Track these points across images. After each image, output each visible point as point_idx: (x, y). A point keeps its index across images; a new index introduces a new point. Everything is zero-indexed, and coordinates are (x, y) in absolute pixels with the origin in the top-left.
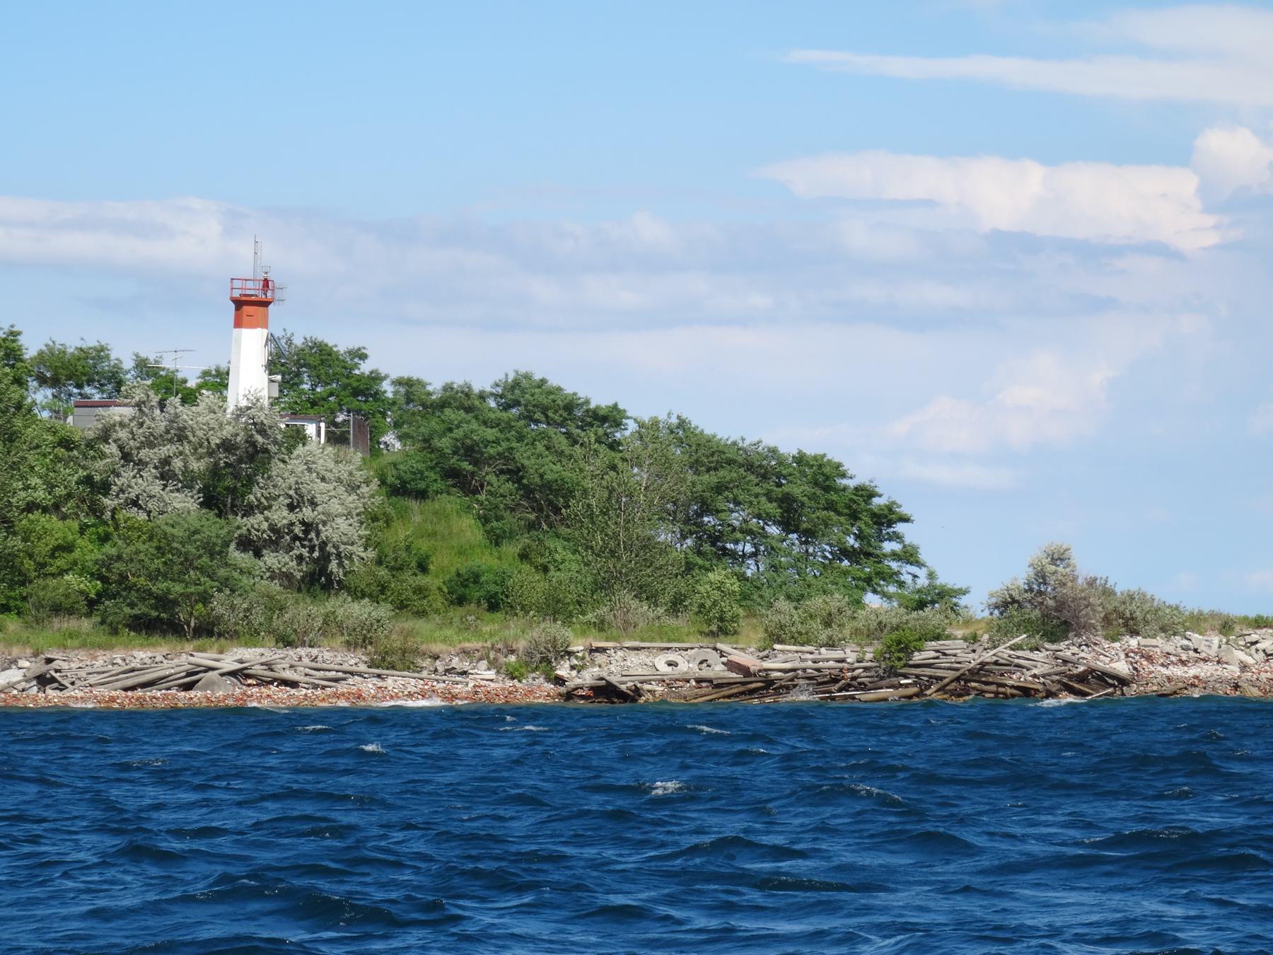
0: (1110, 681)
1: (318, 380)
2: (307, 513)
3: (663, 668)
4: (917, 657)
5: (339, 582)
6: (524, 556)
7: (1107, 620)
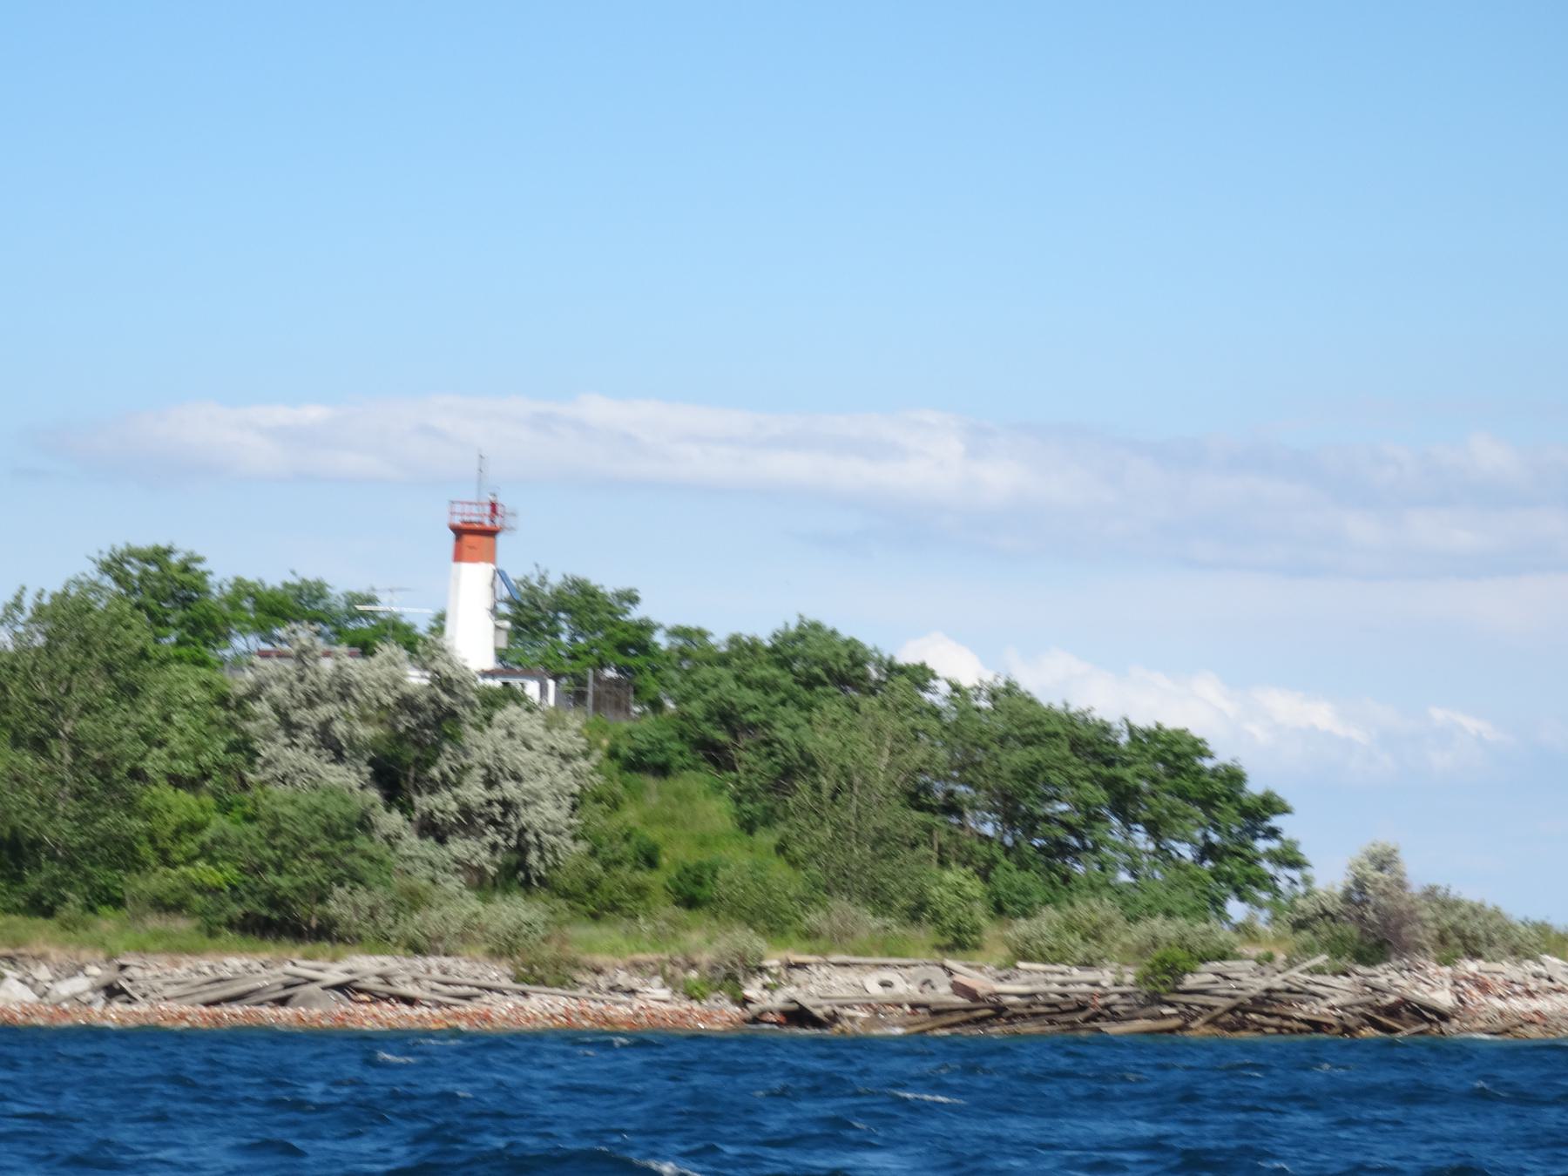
0: (1428, 1015)
1: (580, 627)
2: (510, 789)
3: (875, 989)
4: (1190, 981)
5: (540, 879)
6: (781, 849)
7: (1442, 940)
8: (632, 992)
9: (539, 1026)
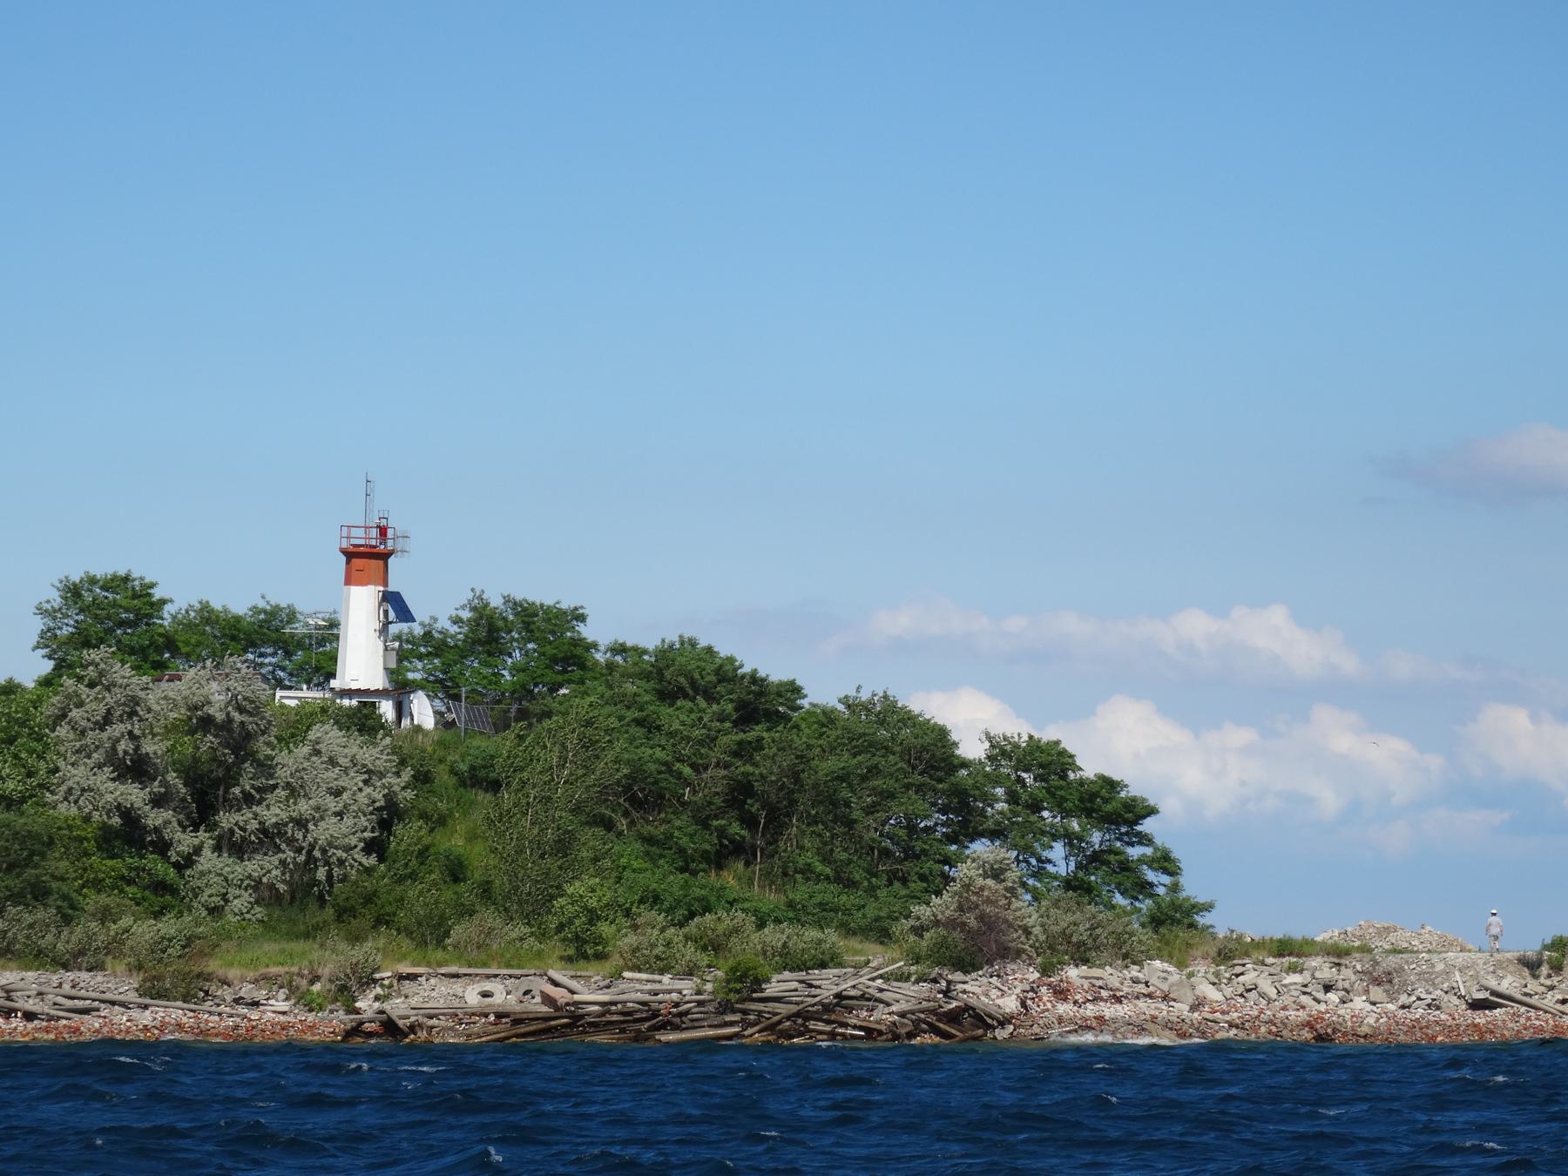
8: (256, 1004)
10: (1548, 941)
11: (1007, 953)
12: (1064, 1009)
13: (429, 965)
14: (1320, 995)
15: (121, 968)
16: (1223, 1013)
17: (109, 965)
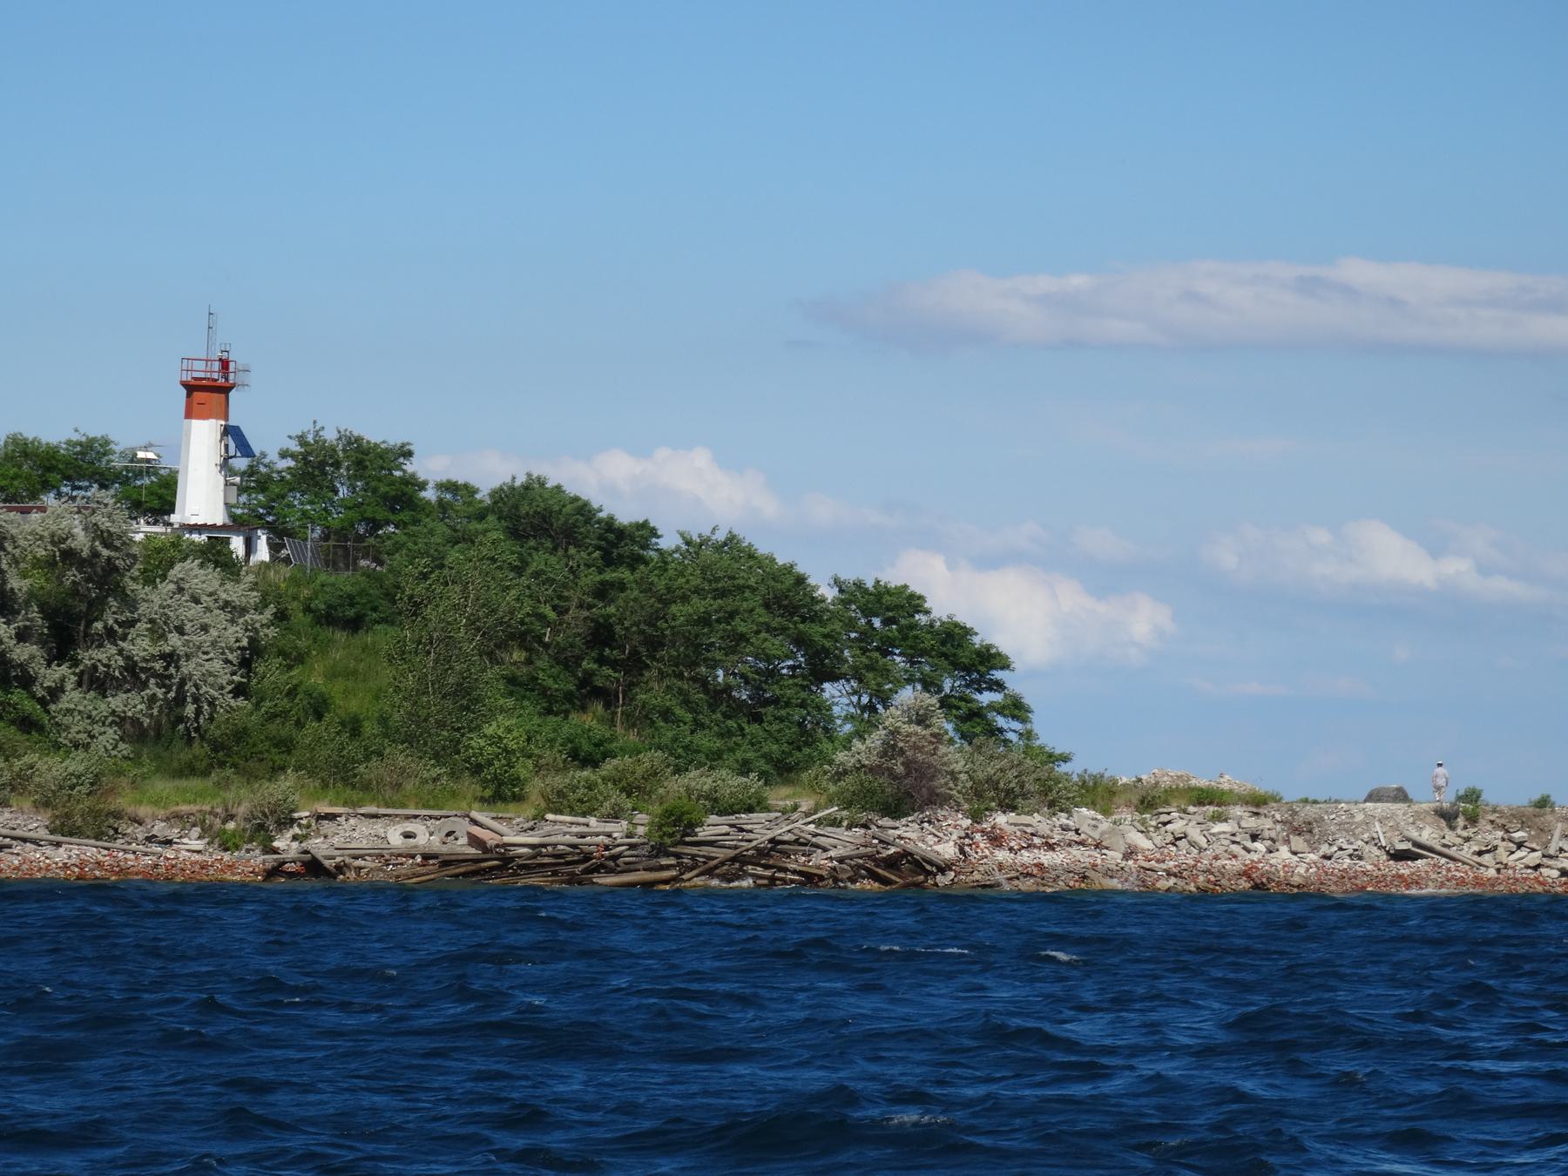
2: (174, 640)
9: (50, 875)
10: (1462, 792)
11: (936, 799)
12: (1002, 855)
13: (345, 804)
14: (1249, 844)
15: (27, 805)
16: (1158, 861)
17: (13, 801)
